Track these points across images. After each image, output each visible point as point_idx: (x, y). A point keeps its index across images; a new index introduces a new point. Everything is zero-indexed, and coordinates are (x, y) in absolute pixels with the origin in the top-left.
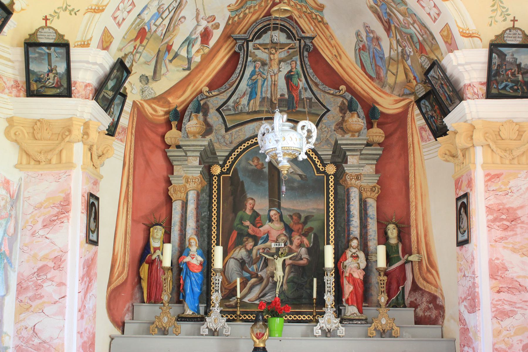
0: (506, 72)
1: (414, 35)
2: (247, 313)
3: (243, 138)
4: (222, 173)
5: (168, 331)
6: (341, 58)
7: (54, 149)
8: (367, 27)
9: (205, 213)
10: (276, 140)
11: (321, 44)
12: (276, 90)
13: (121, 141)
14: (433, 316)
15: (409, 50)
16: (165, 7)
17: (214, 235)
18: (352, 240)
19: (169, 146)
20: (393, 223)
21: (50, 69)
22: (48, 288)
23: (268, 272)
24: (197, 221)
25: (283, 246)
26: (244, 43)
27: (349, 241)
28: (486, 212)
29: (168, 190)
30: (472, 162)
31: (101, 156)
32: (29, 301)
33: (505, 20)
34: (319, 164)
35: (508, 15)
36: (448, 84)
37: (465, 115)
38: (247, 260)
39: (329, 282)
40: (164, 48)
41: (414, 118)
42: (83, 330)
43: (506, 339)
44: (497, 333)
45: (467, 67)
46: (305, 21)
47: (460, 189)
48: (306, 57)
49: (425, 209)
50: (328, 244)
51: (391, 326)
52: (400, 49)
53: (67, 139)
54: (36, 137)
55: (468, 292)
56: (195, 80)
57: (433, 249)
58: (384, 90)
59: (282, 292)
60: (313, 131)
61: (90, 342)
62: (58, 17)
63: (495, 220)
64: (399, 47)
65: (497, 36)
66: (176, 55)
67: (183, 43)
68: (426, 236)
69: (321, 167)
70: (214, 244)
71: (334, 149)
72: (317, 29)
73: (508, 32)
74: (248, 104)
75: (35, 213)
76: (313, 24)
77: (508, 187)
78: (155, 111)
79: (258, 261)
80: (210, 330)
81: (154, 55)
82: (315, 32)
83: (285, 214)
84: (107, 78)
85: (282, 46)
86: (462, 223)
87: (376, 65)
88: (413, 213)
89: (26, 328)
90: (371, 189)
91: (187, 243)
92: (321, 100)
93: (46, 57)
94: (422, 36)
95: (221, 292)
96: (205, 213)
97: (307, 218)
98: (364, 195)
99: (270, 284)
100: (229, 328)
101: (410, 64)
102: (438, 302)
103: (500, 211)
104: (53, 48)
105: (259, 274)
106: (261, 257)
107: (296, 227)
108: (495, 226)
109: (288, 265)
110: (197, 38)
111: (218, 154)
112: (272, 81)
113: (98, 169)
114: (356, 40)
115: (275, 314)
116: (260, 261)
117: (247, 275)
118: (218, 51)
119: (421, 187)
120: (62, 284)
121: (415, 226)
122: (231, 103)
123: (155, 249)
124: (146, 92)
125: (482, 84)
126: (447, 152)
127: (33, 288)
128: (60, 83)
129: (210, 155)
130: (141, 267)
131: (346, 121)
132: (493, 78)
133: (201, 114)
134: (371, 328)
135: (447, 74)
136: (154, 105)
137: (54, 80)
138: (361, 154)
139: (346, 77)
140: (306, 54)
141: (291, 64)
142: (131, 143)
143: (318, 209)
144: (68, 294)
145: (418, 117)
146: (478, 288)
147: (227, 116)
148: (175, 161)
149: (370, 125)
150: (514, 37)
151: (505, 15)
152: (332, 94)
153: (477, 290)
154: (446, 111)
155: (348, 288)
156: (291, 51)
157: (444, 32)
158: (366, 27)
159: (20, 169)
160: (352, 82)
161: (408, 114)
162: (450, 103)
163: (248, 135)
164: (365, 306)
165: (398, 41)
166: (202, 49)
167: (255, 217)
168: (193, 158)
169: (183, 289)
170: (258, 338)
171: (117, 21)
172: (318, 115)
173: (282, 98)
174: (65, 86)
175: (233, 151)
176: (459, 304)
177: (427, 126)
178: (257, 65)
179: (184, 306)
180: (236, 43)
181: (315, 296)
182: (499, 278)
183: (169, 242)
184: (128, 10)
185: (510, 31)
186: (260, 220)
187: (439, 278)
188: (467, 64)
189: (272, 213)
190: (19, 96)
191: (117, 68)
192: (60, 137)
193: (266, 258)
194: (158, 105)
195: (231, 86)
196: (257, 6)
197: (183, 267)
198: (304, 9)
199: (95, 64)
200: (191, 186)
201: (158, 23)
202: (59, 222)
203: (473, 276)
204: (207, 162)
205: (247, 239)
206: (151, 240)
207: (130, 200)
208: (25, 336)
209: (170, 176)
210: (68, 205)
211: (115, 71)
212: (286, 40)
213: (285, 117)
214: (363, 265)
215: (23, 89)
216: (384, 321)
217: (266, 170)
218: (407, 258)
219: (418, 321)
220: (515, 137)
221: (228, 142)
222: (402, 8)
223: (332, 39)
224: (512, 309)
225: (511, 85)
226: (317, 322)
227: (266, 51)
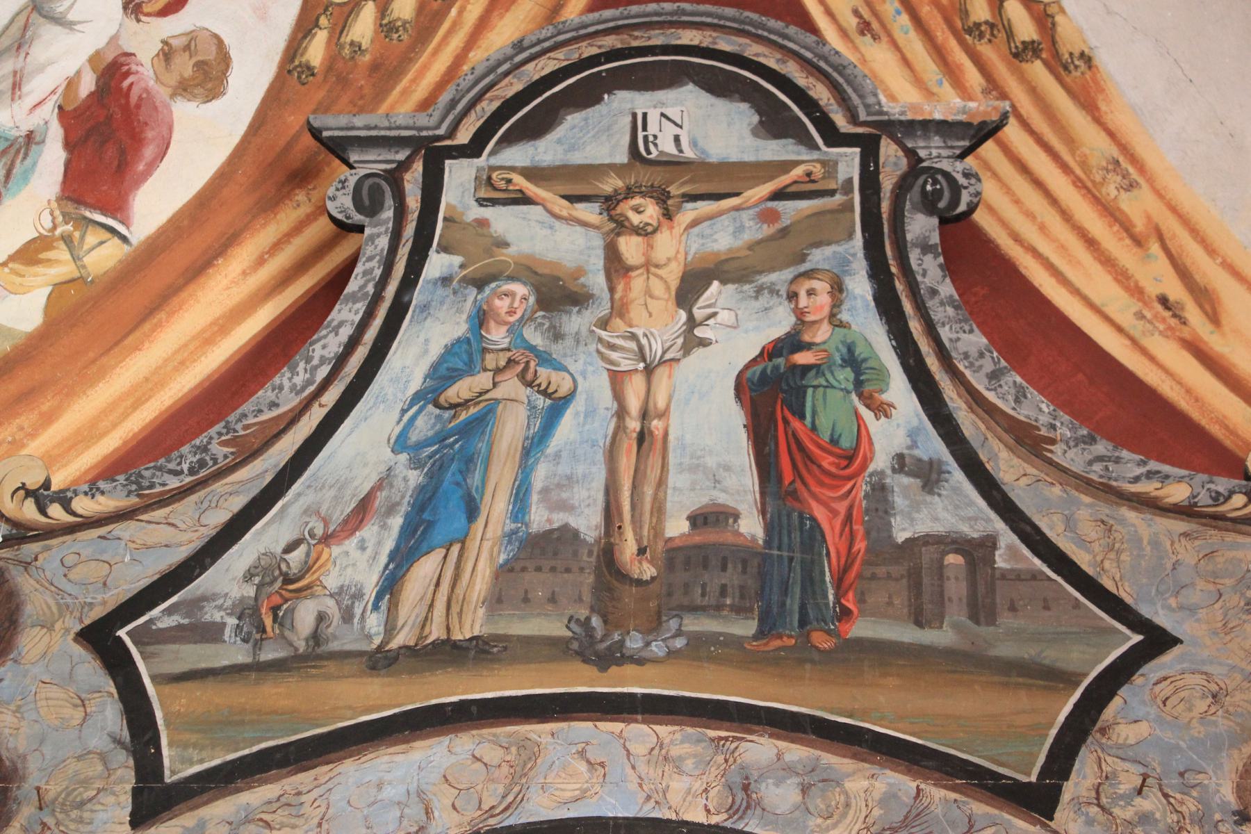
6: (1214, 319)
11: (1042, 228)
12: (653, 474)
26: (404, 166)
46: (906, 62)
48: (926, 248)
92: (1083, 560)
110: (30, 137)
118: (198, 269)
140: (920, 226)
141: (793, 296)
147: (167, 689)
156: (791, 210)
166: (67, 239)
172: (1060, 679)
173: (710, 536)
178: (502, 305)
195: (248, 453)
212: (750, 141)
223: (1131, 186)
227: (589, 212)
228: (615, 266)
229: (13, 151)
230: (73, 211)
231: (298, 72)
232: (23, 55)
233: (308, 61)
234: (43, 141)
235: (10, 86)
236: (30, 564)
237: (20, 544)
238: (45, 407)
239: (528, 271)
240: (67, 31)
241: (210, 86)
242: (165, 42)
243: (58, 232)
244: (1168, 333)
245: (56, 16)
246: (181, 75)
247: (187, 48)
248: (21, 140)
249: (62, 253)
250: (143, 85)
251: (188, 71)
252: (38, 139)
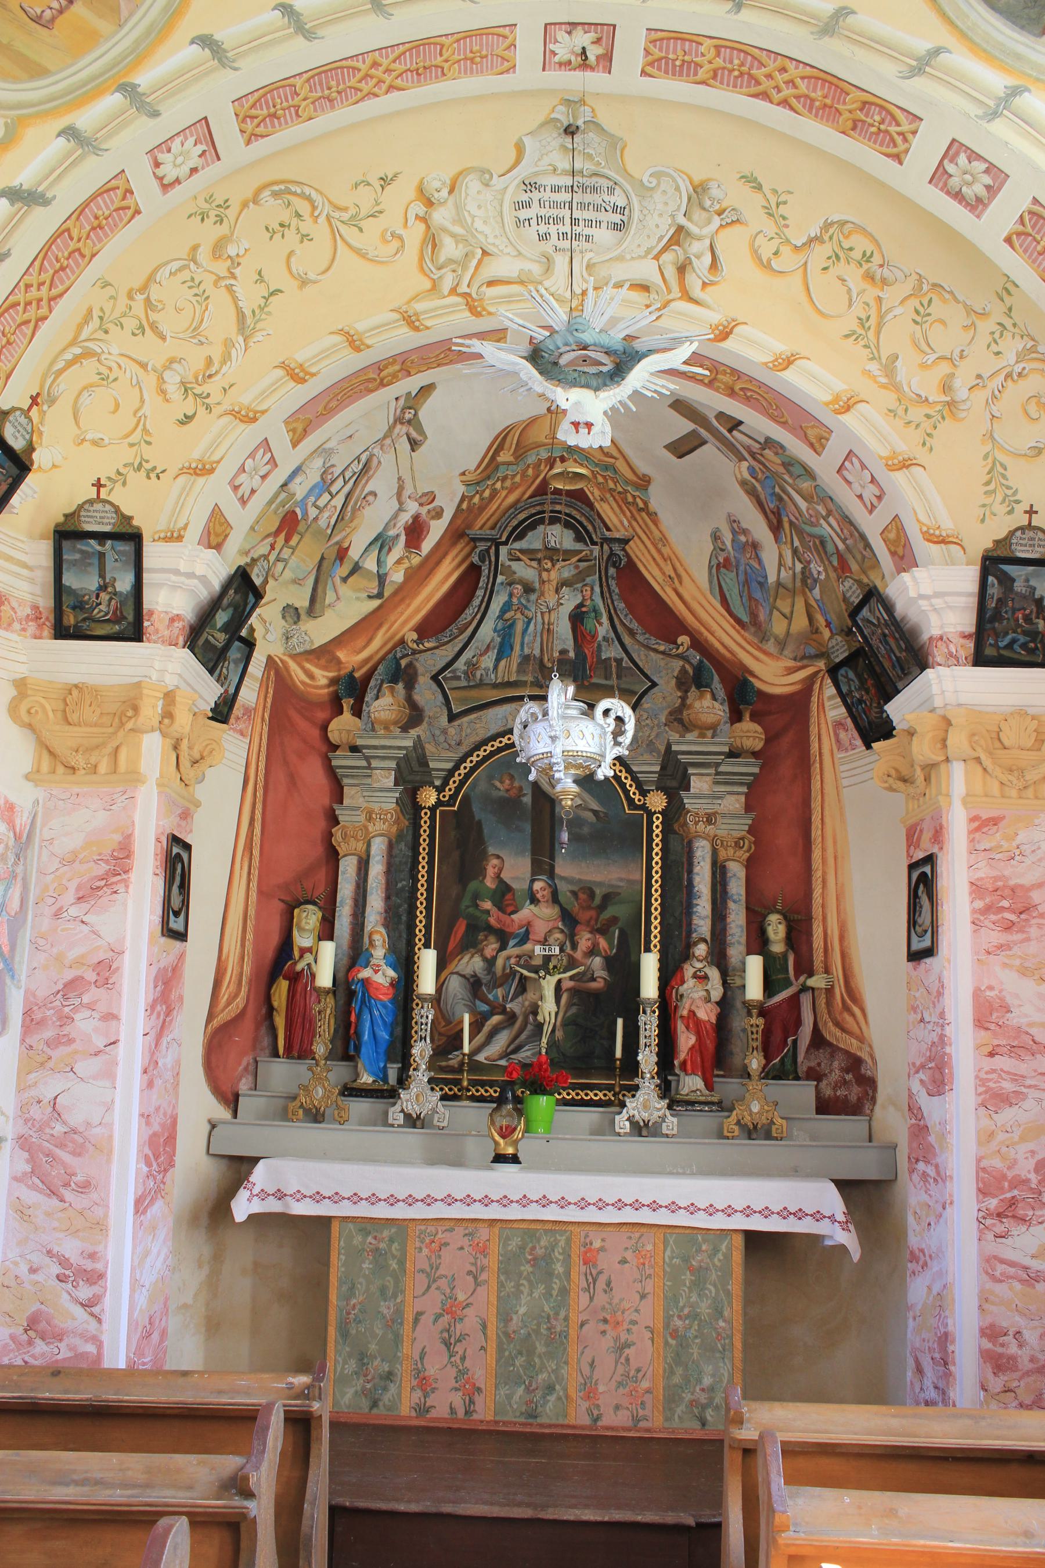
0: (1014, 613)
1: (828, 539)
2: (483, 1084)
3: (483, 734)
4: (439, 803)
5: (323, 1115)
6: (681, 583)
7: (103, 745)
8: (735, 521)
9: (404, 883)
10: (551, 737)
13: (242, 734)
14: (853, 1098)
15: (816, 568)
16: (337, 471)
17: (420, 926)
18: (696, 944)
19: (335, 748)
20: (778, 912)
21: (102, 583)
22: (85, 1024)
23: (527, 1003)
24: (388, 898)
25: (557, 952)
26: (490, 547)
27: (689, 946)
28: (971, 894)
29: (331, 835)
30: (944, 791)
31: (197, 762)
32: (46, 1049)
33: (1010, 512)
34: (633, 790)
35: (1018, 502)
36: (897, 635)
37: (930, 698)
38: (485, 978)
39: (648, 1027)
40: (332, 554)
41: (823, 705)
42: (152, 1110)
43: (1004, 1149)
44: (986, 1137)
45: (937, 602)
47: (917, 846)
48: (613, 578)
49: (843, 885)
50: (648, 950)
51: (770, 1117)
52: (799, 567)
53: (130, 725)
54: (70, 720)
55: (928, 1054)
56: (392, 618)
57: (856, 969)
58: (764, 647)
59: (552, 1044)
60: (626, 720)
61: (166, 1135)
62: (124, 484)
63: (987, 910)
64: (797, 563)
65: (997, 542)
66: (356, 568)
68: (842, 938)
69: (637, 797)
70: (420, 945)
71: (663, 760)
72: (634, 524)
73: (1019, 533)
74: (496, 667)
75: (61, 871)
76: (628, 514)
77: (1014, 844)
78: (311, 676)
79: (506, 981)
80: (408, 1116)
82: (631, 530)
83: (563, 887)
84: (214, 605)
85: (568, 554)
86: (920, 915)
87: (750, 598)
88: (817, 893)
89: (39, 1102)
90: (736, 843)
91: (366, 940)
92: (640, 664)
93: (95, 561)
94: (844, 541)
95: (432, 1040)
96: (404, 883)
97: (607, 899)
98: (722, 854)
99: (530, 1027)
100: (444, 1114)
101: (818, 597)
102: (863, 1071)
103: (998, 893)
104: (109, 543)
105: (508, 1006)
106: (513, 973)
107: (584, 916)
108: (987, 923)
109: (566, 990)
111: (432, 765)
112: (543, 623)
113: (191, 788)
114: (712, 548)
115: (539, 1088)
116: (510, 981)
117: (484, 1008)
118: (439, 562)
119: (835, 843)
120: (110, 1017)
121: (820, 918)
122: (460, 664)
123: (303, 951)
124: (295, 640)
125: (965, 637)
126: (893, 773)
127: (54, 1022)
128: (121, 612)
129: (416, 768)
130: (275, 986)
131: (690, 707)
132: (988, 626)
133: (400, 687)
134: (729, 1120)
135: (895, 614)
136: (308, 666)
137: (109, 605)
138: (717, 773)
139: (690, 619)
142: (261, 739)
143: (629, 881)
144: (122, 1037)
145: (832, 702)
146: (950, 1045)
148: (347, 776)
149: (736, 716)
150: (1030, 545)
151: (1011, 502)
152: (663, 653)
153: (948, 1050)
154: (889, 689)
155: (686, 1040)
156: (583, 565)
157: (890, 532)
158: (733, 522)
159: (36, 783)
160: (703, 630)
161: (811, 696)
162: (900, 673)
163: (494, 730)
164: (718, 1076)
165: (795, 551)
167: (503, 894)
168: (382, 772)
169: (356, 1032)
170: (503, 1137)
171: (240, 495)
174: (131, 618)
175: (463, 759)
176: (909, 1076)
177: (849, 720)
178: (515, 591)
179: (356, 1067)
180: (476, 547)
181: (618, 1054)
182: (993, 1027)
183: (331, 938)
184: (262, 473)
185: (1023, 533)
186: (514, 899)
187: (866, 1022)
188: (937, 595)
189: (538, 886)
190: (40, 638)
191: (234, 586)
192: (117, 720)
193: (522, 974)
194: (317, 666)
195: (462, 632)
196: (519, 476)
197: (358, 988)
198: (611, 485)
199: (191, 575)
200: (377, 827)
201: (321, 503)
202: (109, 892)
203: (941, 1021)
204: (409, 782)
205: (486, 937)
206: (295, 933)
207: (256, 852)
208: (37, 1117)
209: (335, 806)
210: (128, 857)
211: (231, 592)
213: (571, 689)
214: (717, 993)
215: (47, 623)
216: (755, 1108)
217: (527, 800)
218: (805, 982)
219: (824, 1107)
220: (1030, 743)
221: (453, 743)
222: (806, 485)
224: (1017, 1089)
225: (1022, 639)
226: (623, 1105)
227: (534, 564)
228: (543, 582)
239: (521, 582)
244: (670, 586)
249: (406, 561)
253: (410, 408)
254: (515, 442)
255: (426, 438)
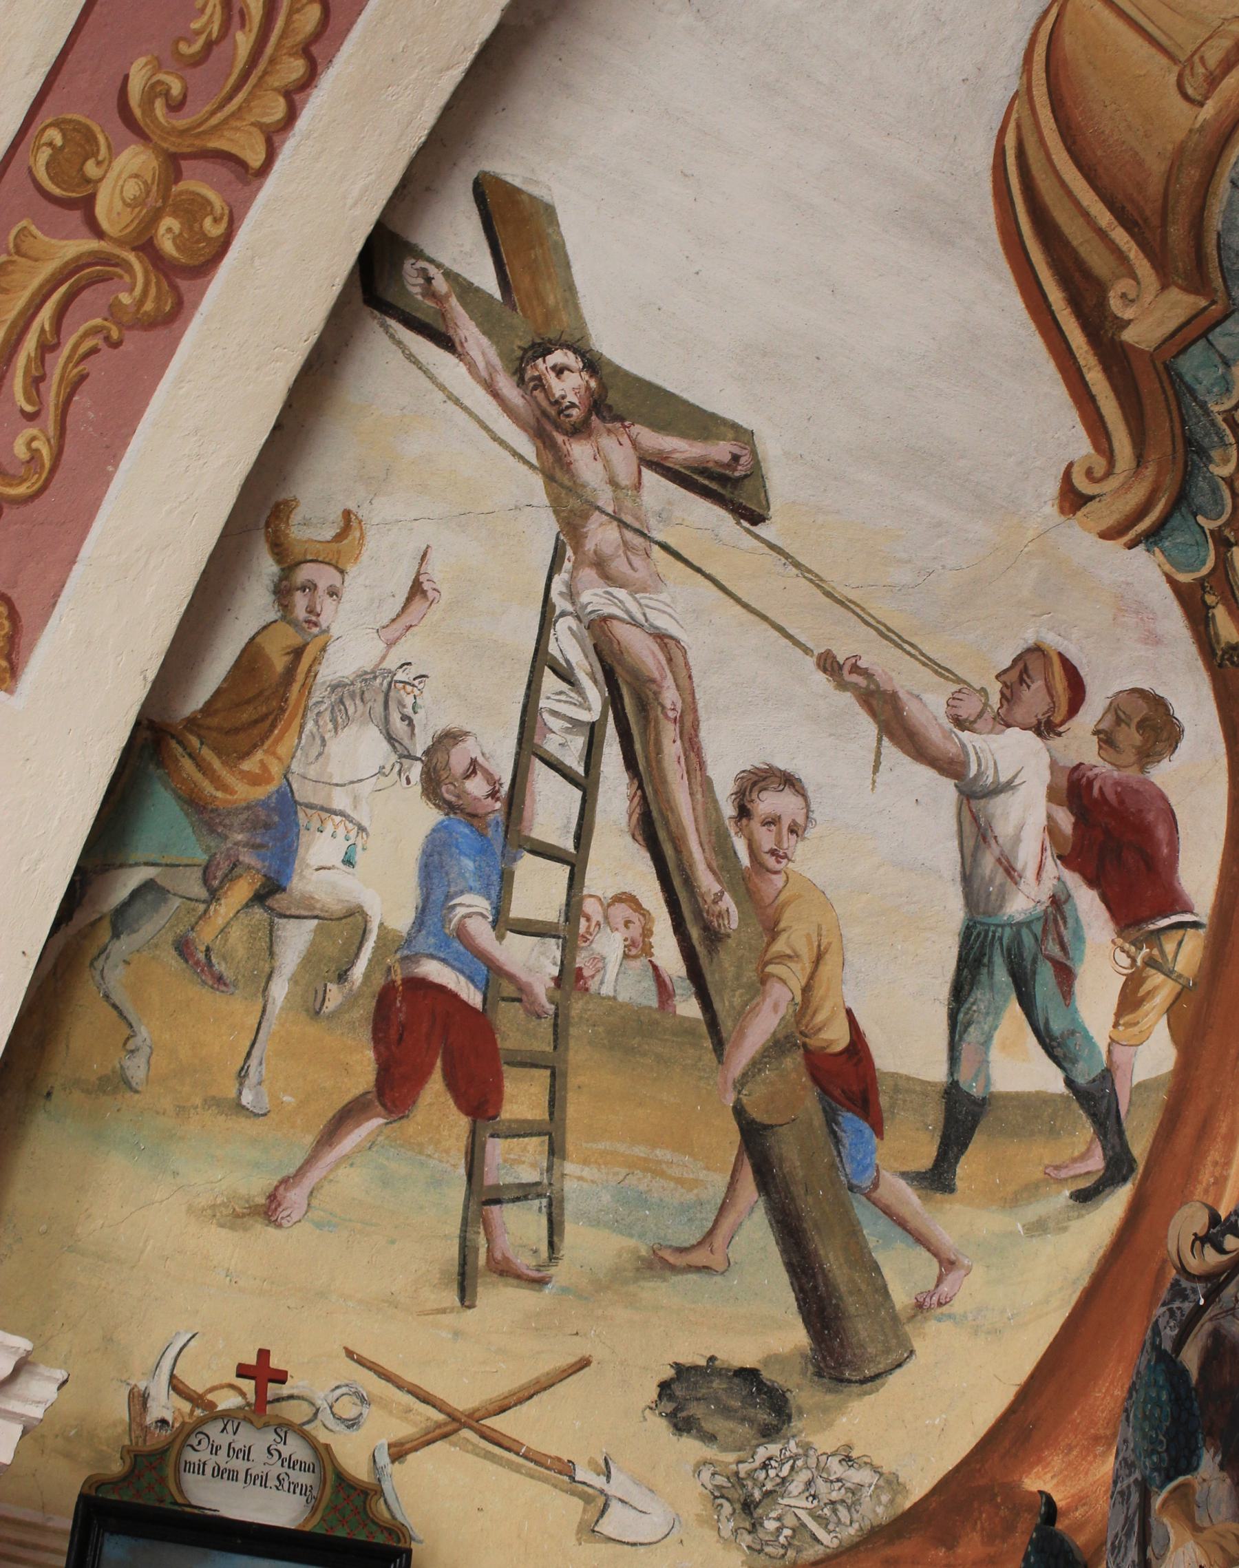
67: (960, 992)
81: (721, 1181)
124: (795, 1501)
166: (1150, 963)
229: (1051, 924)
230: (1138, 934)
231: (1228, 660)
232: (993, 842)
233: (1228, 643)
234: (1069, 896)
235: (1005, 874)
236: (1234, 1309)
237: (1218, 1295)
238: (1224, 1129)
240: (1011, 792)
241: (1165, 735)
242: (1096, 732)
243: (1139, 962)
245: (991, 788)
246: (1133, 746)
247: (1119, 721)
248: (1050, 909)
249: (1156, 978)
250: (1110, 782)
251: (1137, 739)
252: (1063, 898)
253: (544, 350)
254: (1104, 217)
255: (743, 435)
